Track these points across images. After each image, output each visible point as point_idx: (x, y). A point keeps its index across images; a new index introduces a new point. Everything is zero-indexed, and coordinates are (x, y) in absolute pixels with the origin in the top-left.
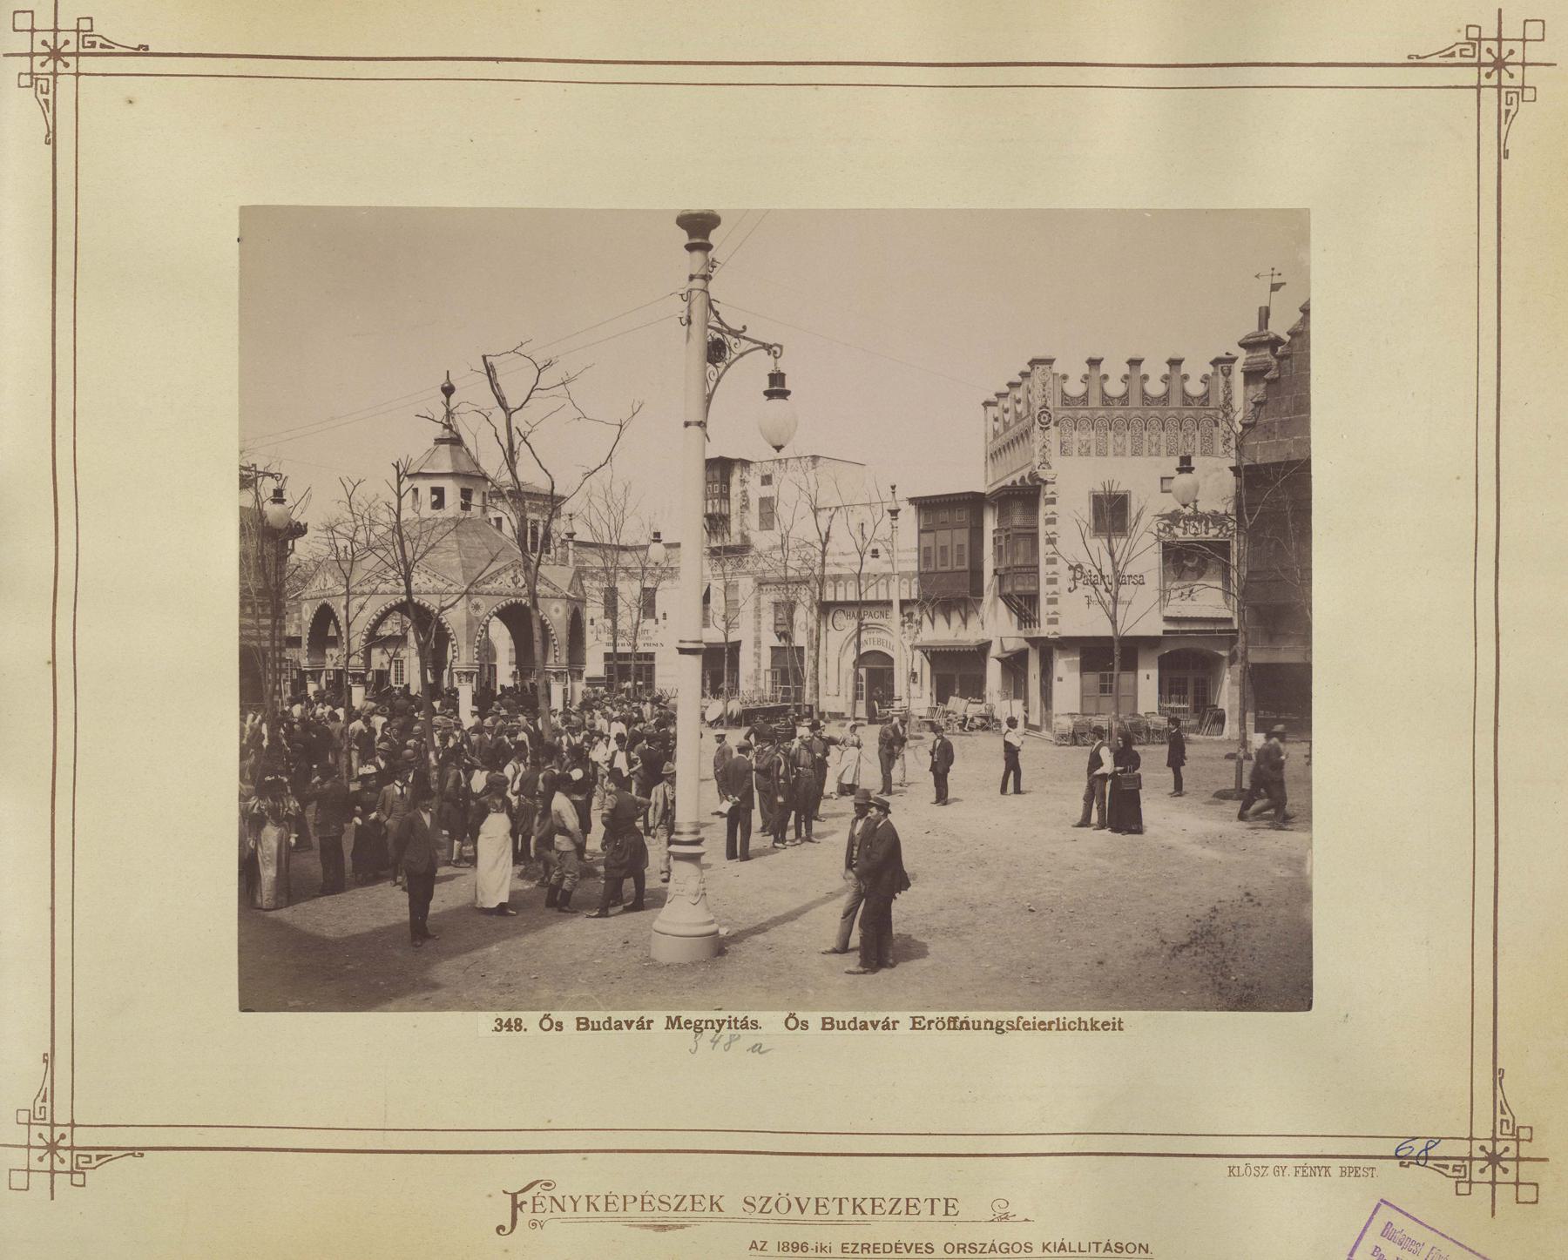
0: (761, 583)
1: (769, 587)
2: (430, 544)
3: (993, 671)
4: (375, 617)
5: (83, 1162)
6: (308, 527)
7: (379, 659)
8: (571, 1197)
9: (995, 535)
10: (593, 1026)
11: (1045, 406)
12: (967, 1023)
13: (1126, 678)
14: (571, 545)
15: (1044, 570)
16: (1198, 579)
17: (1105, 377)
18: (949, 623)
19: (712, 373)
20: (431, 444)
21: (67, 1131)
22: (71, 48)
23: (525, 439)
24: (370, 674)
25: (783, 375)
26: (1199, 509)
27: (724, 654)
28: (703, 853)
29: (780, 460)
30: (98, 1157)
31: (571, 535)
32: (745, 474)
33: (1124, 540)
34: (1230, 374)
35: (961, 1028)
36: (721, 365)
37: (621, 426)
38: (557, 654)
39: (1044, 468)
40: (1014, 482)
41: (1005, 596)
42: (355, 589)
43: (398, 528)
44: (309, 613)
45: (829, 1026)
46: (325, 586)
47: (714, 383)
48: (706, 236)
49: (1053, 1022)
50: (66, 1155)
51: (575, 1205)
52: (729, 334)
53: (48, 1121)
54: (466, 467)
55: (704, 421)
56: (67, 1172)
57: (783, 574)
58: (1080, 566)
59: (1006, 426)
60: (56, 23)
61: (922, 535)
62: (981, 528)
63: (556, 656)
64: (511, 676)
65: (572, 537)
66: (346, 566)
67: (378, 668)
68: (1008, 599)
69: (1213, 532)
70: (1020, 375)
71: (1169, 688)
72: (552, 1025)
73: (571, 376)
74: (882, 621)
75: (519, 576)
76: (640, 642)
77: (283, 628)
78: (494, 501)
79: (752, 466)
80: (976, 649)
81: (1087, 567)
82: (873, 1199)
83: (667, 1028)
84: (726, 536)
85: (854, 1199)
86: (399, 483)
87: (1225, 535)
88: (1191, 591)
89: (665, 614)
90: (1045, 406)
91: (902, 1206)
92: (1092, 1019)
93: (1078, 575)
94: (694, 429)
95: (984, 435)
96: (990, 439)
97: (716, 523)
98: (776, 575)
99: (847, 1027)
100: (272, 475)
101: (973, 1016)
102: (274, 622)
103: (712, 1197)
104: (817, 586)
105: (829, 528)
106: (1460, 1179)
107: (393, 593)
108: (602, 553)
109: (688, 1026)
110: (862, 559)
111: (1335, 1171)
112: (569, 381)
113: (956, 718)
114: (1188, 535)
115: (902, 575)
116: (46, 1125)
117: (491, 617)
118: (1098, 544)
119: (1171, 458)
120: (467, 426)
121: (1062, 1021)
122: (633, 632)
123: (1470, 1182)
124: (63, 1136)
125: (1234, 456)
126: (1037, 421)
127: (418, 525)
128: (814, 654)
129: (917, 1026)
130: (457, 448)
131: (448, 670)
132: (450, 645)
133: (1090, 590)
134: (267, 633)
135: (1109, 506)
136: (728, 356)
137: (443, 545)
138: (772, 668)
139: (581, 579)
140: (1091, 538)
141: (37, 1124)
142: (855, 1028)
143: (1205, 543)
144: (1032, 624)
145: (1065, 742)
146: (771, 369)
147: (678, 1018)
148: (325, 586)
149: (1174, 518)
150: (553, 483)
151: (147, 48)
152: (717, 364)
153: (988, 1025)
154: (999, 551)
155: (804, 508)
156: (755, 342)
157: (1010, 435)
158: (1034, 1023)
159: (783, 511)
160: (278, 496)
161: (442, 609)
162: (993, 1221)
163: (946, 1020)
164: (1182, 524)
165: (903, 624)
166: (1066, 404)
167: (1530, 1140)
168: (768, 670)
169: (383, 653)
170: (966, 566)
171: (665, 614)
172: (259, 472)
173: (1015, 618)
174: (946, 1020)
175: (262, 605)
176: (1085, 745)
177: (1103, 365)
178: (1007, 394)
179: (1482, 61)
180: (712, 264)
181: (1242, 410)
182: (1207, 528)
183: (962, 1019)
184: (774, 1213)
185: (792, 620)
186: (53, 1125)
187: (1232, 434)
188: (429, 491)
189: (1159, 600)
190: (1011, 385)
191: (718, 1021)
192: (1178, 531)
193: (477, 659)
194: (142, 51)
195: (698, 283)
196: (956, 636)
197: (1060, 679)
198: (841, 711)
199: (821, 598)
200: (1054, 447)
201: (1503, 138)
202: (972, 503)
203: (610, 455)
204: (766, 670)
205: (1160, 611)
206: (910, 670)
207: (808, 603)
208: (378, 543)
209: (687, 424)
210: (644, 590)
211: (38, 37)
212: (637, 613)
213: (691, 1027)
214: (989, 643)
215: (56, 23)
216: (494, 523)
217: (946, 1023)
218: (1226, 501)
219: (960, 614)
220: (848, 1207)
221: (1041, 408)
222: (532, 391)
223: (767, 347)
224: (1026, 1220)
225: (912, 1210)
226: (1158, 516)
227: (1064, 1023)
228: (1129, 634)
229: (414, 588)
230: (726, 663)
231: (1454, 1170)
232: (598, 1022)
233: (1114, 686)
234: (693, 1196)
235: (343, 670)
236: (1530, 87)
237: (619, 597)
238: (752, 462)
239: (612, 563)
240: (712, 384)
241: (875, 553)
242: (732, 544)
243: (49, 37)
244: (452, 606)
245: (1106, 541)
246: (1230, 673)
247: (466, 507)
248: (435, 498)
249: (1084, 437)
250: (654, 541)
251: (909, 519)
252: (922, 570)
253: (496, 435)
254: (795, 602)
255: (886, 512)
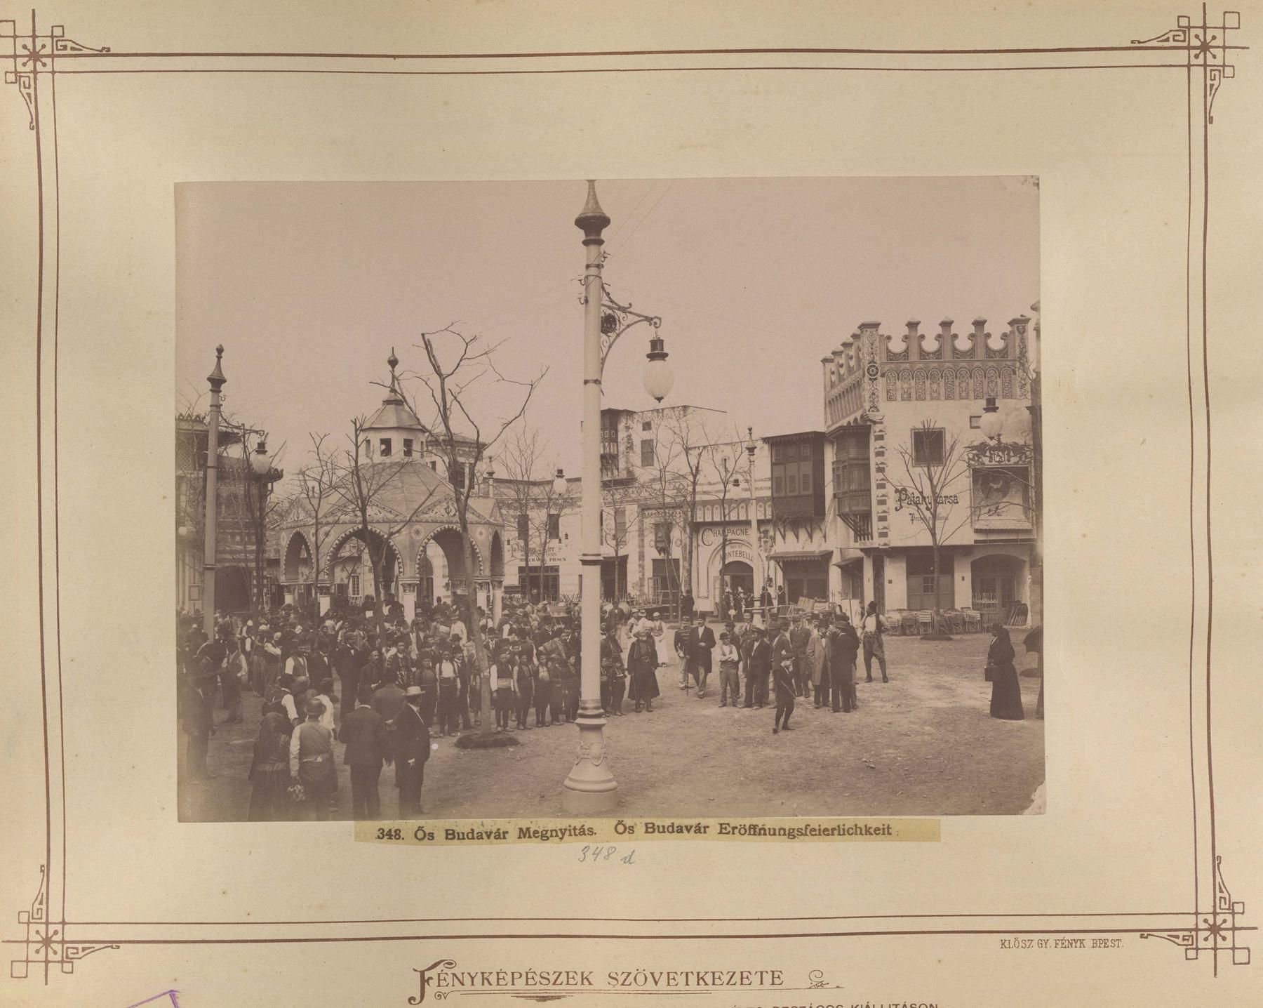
0: (644, 509)
1: (650, 512)
2: (381, 483)
3: (835, 577)
4: (337, 542)
5: (71, 953)
6: (284, 473)
7: (340, 575)
8: (469, 974)
9: (834, 466)
10: (459, 836)
11: (873, 361)
12: (765, 830)
13: (944, 580)
14: (491, 482)
15: (875, 493)
16: (1003, 497)
17: (922, 337)
18: (797, 537)
19: (605, 342)
20: (380, 406)
21: (59, 927)
22: (48, 51)
23: (455, 398)
24: (333, 587)
25: (662, 341)
26: (1002, 440)
27: (614, 565)
28: (603, 725)
29: (658, 411)
30: (84, 949)
31: (491, 474)
32: (630, 422)
33: (941, 468)
34: (1024, 332)
35: (760, 834)
36: (613, 335)
37: (532, 385)
38: (482, 568)
39: (873, 411)
40: (849, 423)
41: (843, 515)
42: (322, 520)
43: (356, 471)
44: (286, 540)
45: (651, 830)
46: (298, 518)
47: (607, 348)
48: (599, 233)
49: (835, 829)
50: (58, 947)
51: (473, 982)
52: (619, 310)
53: (44, 920)
54: (407, 422)
55: (599, 379)
56: (59, 962)
57: (661, 500)
58: (904, 490)
59: (841, 378)
60: (34, 30)
61: (774, 467)
62: (823, 461)
63: (481, 570)
64: (445, 587)
65: (492, 475)
66: (315, 502)
67: (339, 582)
68: (844, 517)
69: (1014, 460)
70: (852, 337)
71: (980, 586)
72: (425, 836)
73: (492, 346)
74: (743, 537)
75: (451, 507)
76: (547, 558)
77: (264, 552)
78: (430, 448)
79: (636, 416)
80: (820, 559)
81: (910, 491)
82: (714, 973)
83: (520, 837)
84: (615, 472)
85: (698, 973)
86: (357, 436)
87: (1024, 461)
88: (997, 508)
89: (567, 535)
90: (873, 361)
91: (737, 978)
92: (866, 826)
93: (903, 497)
94: (591, 386)
95: (823, 386)
96: (828, 389)
97: (608, 461)
98: (656, 502)
99: (666, 830)
100: (257, 432)
101: (770, 822)
102: (258, 548)
103: (582, 973)
104: (689, 510)
105: (698, 463)
106: (1189, 947)
107: (351, 523)
108: (516, 487)
109: (537, 835)
110: (725, 487)
111: (1088, 943)
112: (490, 351)
113: (805, 614)
114: (994, 463)
115: (759, 500)
116: (42, 923)
117: (429, 540)
118: (919, 472)
119: (977, 400)
120: (409, 388)
121: (841, 827)
122: (542, 549)
123: (1197, 949)
124: (56, 932)
125: (1030, 398)
126: (866, 373)
127: (371, 469)
128: (687, 565)
129: (724, 831)
130: (400, 407)
131: (394, 583)
132: (396, 562)
133: (913, 509)
134: (252, 556)
135: (928, 441)
136: (618, 327)
137: (391, 483)
138: (654, 576)
139: (500, 508)
140: (913, 467)
141: (35, 923)
142: (673, 832)
143: (1008, 469)
144: (866, 537)
145: (895, 633)
146: (652, 336)
147: (528, 829)
148: (298, 518)
149: (981, 449)
150: (478, 432)
151: (109, 49)
152: (609, 334)
153: (782, 832)
154: (837, 480)
155: (678, 448)
156: (639, 316)
157: (845, 384)
158: (820, 829)
159: (661, 452)
160: (261, 449)
161: (392, 534)
162: (810, 988)
163: (747, 827)
164: (988, 454)
165: (760, 539)
166: (890, 360)
167: (1243, 913)
168: (651, 578)
169: (342, 570)
170: (811, 492)
171: (567, 535)
172: (247, 430)
173: (852, 533)
174: (747, 827)
175: (248, 535)
176: (912, 635)
177: (920, 328)
178: (842, 352)
179: (1192, 44)
180: (604, 256)
181: (1035, 361)
182: (1009, 456)
183: (760, 826)
184: (634, 986)
185: (669, 538)
186: (47, 923)
187: (1028, 380)
188: (379, 441)
189: (971, 515)
190: (845, 345)
191: (486, 833)
192: (986, 460)
193: (418, 573)
194: (105, 52)
195: (593, 271)
196: (803, 548)
197: (890, 582)
198: (710, 610)
199: (692, 519)
200: (882, 394)
201: (1208, 107)
202: (814, 441)
203: (524, 408)
204: (649, 579)
205: (972, 525)
206: (766, 576)
207: (682, 524)
208: (340, 483)
209: (586, 382)
210: (550, 516)
211: (20, 42)
212: (545, 535)
213: (538, 837)
214: (830, 554)
215: (34, 30)
216: (430, 465)
217: (748, 830)
218: (1024, 435)
219: (807, 530)
220: (693, 979)
221: (869, 363)
222: (461, 361)
223: (648, 319)
224: (838, 987)
225: (745, 981)
226: (968, 447)
227: (844, 829)
228: (947, 543)
229: (368, 518)
230: (617, 573)
231: (1184, 940)
232: (463, 833)
233: (935, 587)
234: (568, 973)
235: (313, 584)
236: (1230, 66)
237: (529, 522)
238: (635, 412)
239: (524, 495)
240: (605, 350)
241: (736, 483)
242: (620, 478)
243: (29, 42)
244: (398, 531)
245: (926, 469)
246: (1031, 575)
247: (408, 453)
248: (383, 447)
249: (906, 386)
250: (558, 476)
251: (764, 456)
252: (775, 495)
253: (433, 396)
254: (671, 523)
255: (744, 449)
